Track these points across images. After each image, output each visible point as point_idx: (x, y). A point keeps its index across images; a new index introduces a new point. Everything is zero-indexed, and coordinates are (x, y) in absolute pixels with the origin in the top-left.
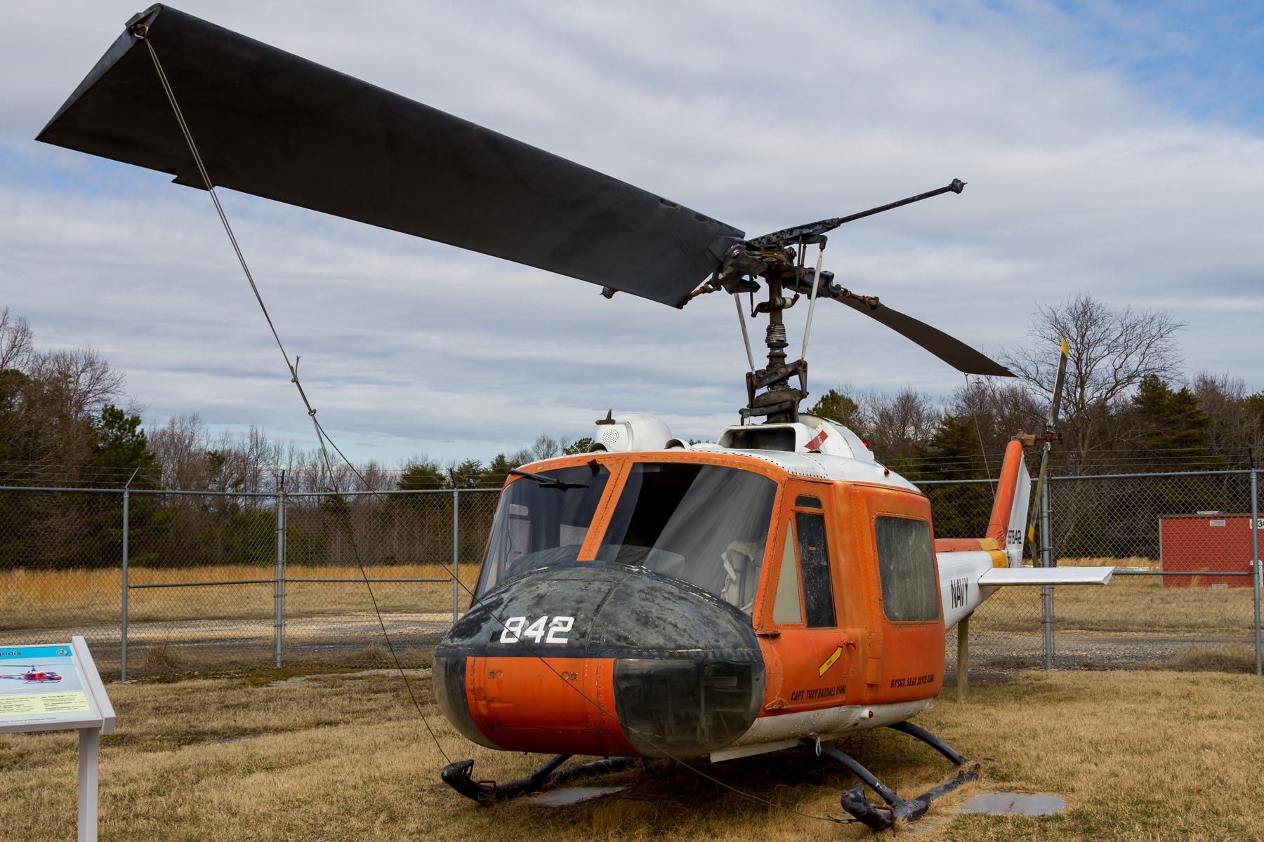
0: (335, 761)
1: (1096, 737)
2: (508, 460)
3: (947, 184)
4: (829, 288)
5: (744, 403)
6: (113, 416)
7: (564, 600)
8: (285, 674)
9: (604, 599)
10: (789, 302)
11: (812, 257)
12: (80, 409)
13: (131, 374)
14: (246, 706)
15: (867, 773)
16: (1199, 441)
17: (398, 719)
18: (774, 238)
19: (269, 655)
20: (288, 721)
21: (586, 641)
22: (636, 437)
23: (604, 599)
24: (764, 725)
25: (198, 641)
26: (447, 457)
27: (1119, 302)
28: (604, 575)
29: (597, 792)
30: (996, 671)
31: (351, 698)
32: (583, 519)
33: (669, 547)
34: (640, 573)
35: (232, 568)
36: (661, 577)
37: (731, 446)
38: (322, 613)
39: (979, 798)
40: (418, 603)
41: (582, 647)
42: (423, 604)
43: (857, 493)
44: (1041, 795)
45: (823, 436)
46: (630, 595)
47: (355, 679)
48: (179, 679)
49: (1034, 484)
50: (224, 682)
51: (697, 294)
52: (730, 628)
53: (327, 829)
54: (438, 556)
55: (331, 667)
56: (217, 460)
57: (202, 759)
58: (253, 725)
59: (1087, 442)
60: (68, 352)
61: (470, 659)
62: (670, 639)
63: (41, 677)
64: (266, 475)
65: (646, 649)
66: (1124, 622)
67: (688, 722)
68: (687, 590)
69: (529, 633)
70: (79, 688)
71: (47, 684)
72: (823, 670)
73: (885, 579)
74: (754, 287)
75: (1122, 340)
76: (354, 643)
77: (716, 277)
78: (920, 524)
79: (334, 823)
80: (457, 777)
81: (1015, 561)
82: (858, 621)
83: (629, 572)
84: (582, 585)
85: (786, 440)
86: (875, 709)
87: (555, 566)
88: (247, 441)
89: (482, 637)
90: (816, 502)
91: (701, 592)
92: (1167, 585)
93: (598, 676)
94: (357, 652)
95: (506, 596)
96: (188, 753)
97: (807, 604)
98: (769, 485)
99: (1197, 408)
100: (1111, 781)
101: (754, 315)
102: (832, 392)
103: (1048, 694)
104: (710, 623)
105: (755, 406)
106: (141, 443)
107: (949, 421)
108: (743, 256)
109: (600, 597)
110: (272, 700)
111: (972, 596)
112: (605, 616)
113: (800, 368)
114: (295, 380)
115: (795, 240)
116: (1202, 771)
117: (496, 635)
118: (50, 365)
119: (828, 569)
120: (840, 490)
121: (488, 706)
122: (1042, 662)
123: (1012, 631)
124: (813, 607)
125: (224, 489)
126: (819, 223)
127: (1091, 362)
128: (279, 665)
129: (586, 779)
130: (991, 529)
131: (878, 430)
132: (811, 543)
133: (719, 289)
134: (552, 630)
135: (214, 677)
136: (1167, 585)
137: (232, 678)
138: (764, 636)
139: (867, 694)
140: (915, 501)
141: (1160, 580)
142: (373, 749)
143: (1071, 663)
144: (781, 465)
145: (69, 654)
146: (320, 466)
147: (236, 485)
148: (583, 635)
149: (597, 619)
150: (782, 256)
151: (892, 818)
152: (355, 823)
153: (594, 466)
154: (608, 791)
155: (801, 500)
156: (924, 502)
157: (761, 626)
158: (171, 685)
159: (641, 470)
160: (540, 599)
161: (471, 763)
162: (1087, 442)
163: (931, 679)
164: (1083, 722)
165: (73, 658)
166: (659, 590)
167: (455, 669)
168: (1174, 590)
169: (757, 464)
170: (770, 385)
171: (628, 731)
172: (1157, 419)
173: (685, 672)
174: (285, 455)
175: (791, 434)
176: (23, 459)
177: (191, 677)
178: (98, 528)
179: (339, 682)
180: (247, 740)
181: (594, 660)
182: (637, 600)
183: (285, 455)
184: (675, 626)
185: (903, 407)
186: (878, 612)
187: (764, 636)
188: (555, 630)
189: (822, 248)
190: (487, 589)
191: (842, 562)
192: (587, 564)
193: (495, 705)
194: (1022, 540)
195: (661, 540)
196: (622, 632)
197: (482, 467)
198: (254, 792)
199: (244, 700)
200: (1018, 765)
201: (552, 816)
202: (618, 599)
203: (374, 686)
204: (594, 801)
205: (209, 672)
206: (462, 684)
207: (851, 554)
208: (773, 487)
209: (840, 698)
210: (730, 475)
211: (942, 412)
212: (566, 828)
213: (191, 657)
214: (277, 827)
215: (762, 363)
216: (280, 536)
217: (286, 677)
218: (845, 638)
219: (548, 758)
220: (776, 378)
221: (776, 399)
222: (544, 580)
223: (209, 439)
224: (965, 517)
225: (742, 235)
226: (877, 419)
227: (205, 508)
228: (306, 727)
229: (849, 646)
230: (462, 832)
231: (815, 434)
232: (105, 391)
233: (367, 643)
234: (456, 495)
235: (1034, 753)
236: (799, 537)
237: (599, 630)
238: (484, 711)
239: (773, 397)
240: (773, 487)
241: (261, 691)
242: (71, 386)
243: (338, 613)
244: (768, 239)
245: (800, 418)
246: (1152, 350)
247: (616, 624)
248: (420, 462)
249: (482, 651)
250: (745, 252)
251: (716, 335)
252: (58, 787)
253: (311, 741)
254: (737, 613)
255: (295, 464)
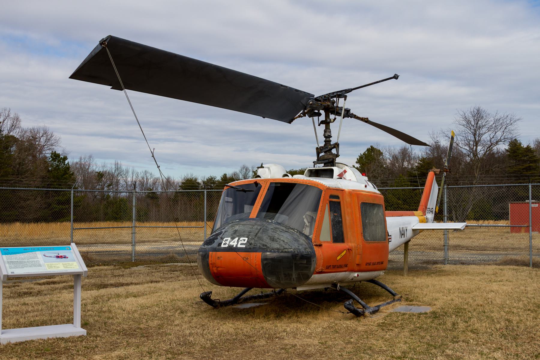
0: (159, 294)
1: (450, 287)
2: (228, 176)
3: (392, 76)
4: (348, 114)
5: (315, 159)
6: (55, 156)
7: (244, 232)
8: (136, 264)
9: (258, 232)
10: (332, 120)
11: (341, 103)
12: (41, 153)
13: (63, 136)
14: (123, 276)
15: (356, 297)
16: (534, 169)
17: (183, 280)
18: (327, 96)
19: (129, 257)
20: (140, 280)
21: (252, 246)
22: (272, 173)
23: (258, 232)
24: (316, 277)
25: (98, 252)
26: (201, 175)
27: (494, 107)
28: (259, 223)
29: (258, 304)
30: (425, 265)
31: (164, 273)
32: (253, 203)
33: (282, 213)
34: (272, 222)
35: (109, 222)
36: (279, 224)
37: (310, 176)
38: (149, 241)
39: (400, 307)
40: (190, 237)
41: (250, 248)
42: (191, 238)
43: (354, 194)
44: (423, 306)
45: (345, 172)
46: (268, 230)
47: (165, 266)
48: (94, 266)
49: (439, 189)
50: (112, 267)
51: (297, 118)
52: (304, 242)
53: (158, 315)
54: (197, 218)
55: (155, 262)
56: (100, 175)
57: (109, 293)
58: (126, 282)
59: (478, 170)
60: (36, 128)
61: (211, 253)
62: (282, 246)
63: (61, 257)
64: (122, 182)
65: (273, 249)
66: (485, 247)
67: (288, 276)
68: (288, 229)
69: (232, 243)
70: (74, 261)
71: (63, 259)
72: (339, 258)
73: (364, 226)
74: (319, 115)
75: (494, 126)
76: (162, 253)
77: (304, 111)
78: (378, 205)
79: (161, 313)
80: (206, 298)
81: (430, 220)
82: (353, 240)
83: (268, 222)
84: (251, 227)
85: (329, 173)
86: (360, 274)
87: (241, 220)
88: (114, 167)
89: (215, 245)
90: (338, 197)
91: (294, 229)
92: (512, 232)
93: (256, 258)
94: (165, 256)
95: (223, 231)
96: (103, 291)
97: (333, 234)
98: (320, 191)
99: (535, 154)
100: (450, 302)
101: (319, 125)
102: (372, 147)
103: (441, 273)
104: (296, 240)
105: (319, 160)
106: (68, 168)
107: (423, 160)
108: (314, 104)
109: (257, 231)
110: (132, 274)
111: (409, 234)
112: (258, 238)
113: (337, 146)
114: (153, 156)
115: (335, 96)
116: (486, 299)
117: (220, 244)
118: (28, 134)
119: (341, 222)
120: (347, 193)
121: (217, 270)
122: (443, 262)
123: (438, 250)
124: (335, 235)
125: (103, 189)
126: (344, 90)
127: (480, 135)
128: (133, 261)
129: (254, 300)
130: (420, 208)
131: (391, 164)
132: (335, 212)
133: (305, 116)
134: (240, 243)
135: (107, 265)
136: (512, 231)
137: (115, 266)
138: (316, 245)
139: (357, 268)
140: (377, 197)
141: (509, 230)
142: (174, 290)
143: (455, 263)
144: (324, 183)
145: (70, 249)
146: (145, 178)
147: (109, 186)
148: (251, 244)
149: (256, 239)
150: (329, 103)
151: (364, 312)
152: (168, 313)
153: (256, 184)
154: (261, 304)
155: (332, 196)
156: (381, 197)
157: (315, 242)
158: (91, 268)
159: (274, 185)
160: (236, 231)
161: (211, 292)
162: (478, 170)
163: (382, 263)
164: (448, 283)
165: (72, 250)
166: (278, 228)
167: (205, 256)
168: (514, 234)
169: (316, 183)
170: (325, 152)
171: (267, 279)
172: (516, 159)
173: (287, 258)
174: (130, 173)
175: (332, 171)
176: (17, 175)
177: (98, 265)
178: (50, 205)
179: (158, 267)
180: (125, 287)
181: (255, 253)
182: (270, 233)
183: (130, 173)
184: (284, 241)
185: (403, 154)
186: (360, 238)
187: (316, 245)
188: (241, 242)
189: (345, 100)
190: (217, 228)
191: (347, 219)
192: (253, 219)
193: (219, 269)
194: (434, 212)
195: (280, 211)
196: (264, 243)
197: (217, 179)
198: (130, 303)
199: (121, 273)
200: (417, 297)
201: (240, 311)
202: (263, 231)
203: (172, 269)
204: (258, 307)
205: (105, 263)
206: (208, 262)
207: (351, 217)
208: (321, 192)
209: (346, 269)
210: (307, 187)
211: (420, 155)
212: (245, 315)
213: (98, 258)
214: (141, 314)
215: (322, 144)
216: (134, 208)
217: (137, 266)
218: (348, 247)
219: (240, 289)
220: (327, 149)
221: (327, 156)
222: (237, 225)
223: (97, 165)
224: (409, 203)
225: (313, 96)
226: (391, 158)
227: (95, 197)
228: (147, 283)
229: (349, 250)
230: (207, 316)
231: (342, 171)
232: (52, 145)
233: (168, 253)
234: (205, 192)
235: (425, 293)
236: (331, 210)
237: (256, 242)
238: (215, 271)
239: (326, 157)
240: (321, 192)
241: (128, 271)
242: (37, 143)
243: (156, 241)
244: (325, 96)
245: (336, 165)
246: (507, 130)
247: (262, 240)
248: (189, 177)
249: (215, 250)
250: (315, 102)
251: (306, 130)
252: (57, 301)
253: (150, 287)
254: (307, 237)
255: (134, 177)
